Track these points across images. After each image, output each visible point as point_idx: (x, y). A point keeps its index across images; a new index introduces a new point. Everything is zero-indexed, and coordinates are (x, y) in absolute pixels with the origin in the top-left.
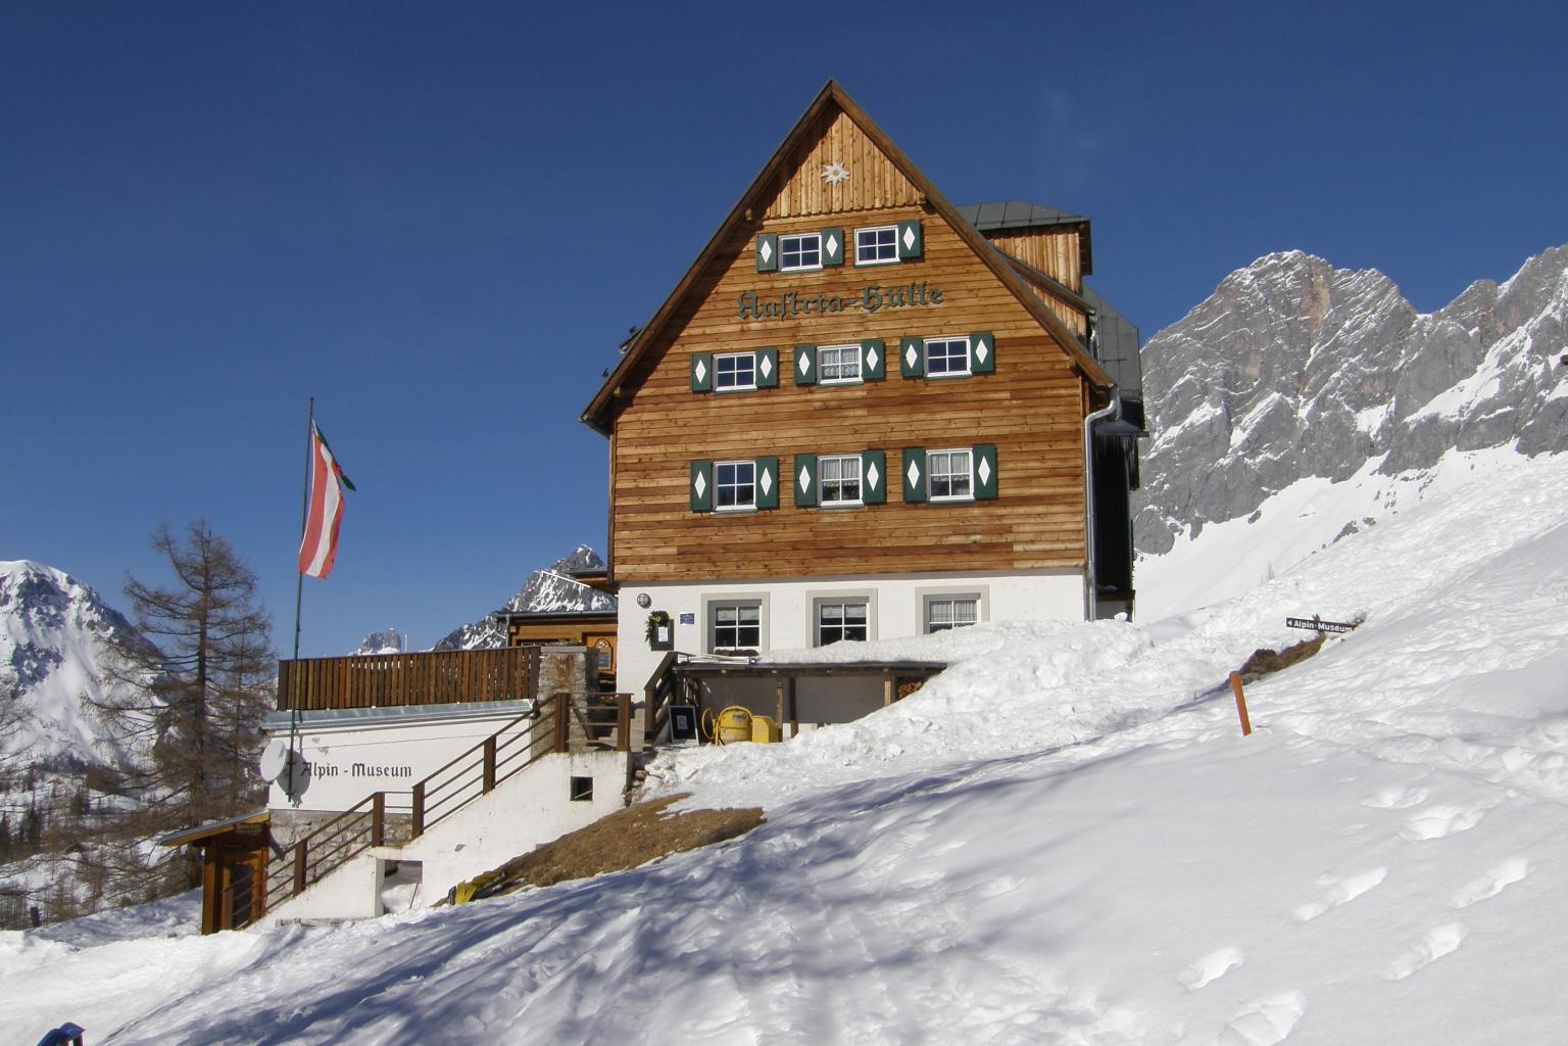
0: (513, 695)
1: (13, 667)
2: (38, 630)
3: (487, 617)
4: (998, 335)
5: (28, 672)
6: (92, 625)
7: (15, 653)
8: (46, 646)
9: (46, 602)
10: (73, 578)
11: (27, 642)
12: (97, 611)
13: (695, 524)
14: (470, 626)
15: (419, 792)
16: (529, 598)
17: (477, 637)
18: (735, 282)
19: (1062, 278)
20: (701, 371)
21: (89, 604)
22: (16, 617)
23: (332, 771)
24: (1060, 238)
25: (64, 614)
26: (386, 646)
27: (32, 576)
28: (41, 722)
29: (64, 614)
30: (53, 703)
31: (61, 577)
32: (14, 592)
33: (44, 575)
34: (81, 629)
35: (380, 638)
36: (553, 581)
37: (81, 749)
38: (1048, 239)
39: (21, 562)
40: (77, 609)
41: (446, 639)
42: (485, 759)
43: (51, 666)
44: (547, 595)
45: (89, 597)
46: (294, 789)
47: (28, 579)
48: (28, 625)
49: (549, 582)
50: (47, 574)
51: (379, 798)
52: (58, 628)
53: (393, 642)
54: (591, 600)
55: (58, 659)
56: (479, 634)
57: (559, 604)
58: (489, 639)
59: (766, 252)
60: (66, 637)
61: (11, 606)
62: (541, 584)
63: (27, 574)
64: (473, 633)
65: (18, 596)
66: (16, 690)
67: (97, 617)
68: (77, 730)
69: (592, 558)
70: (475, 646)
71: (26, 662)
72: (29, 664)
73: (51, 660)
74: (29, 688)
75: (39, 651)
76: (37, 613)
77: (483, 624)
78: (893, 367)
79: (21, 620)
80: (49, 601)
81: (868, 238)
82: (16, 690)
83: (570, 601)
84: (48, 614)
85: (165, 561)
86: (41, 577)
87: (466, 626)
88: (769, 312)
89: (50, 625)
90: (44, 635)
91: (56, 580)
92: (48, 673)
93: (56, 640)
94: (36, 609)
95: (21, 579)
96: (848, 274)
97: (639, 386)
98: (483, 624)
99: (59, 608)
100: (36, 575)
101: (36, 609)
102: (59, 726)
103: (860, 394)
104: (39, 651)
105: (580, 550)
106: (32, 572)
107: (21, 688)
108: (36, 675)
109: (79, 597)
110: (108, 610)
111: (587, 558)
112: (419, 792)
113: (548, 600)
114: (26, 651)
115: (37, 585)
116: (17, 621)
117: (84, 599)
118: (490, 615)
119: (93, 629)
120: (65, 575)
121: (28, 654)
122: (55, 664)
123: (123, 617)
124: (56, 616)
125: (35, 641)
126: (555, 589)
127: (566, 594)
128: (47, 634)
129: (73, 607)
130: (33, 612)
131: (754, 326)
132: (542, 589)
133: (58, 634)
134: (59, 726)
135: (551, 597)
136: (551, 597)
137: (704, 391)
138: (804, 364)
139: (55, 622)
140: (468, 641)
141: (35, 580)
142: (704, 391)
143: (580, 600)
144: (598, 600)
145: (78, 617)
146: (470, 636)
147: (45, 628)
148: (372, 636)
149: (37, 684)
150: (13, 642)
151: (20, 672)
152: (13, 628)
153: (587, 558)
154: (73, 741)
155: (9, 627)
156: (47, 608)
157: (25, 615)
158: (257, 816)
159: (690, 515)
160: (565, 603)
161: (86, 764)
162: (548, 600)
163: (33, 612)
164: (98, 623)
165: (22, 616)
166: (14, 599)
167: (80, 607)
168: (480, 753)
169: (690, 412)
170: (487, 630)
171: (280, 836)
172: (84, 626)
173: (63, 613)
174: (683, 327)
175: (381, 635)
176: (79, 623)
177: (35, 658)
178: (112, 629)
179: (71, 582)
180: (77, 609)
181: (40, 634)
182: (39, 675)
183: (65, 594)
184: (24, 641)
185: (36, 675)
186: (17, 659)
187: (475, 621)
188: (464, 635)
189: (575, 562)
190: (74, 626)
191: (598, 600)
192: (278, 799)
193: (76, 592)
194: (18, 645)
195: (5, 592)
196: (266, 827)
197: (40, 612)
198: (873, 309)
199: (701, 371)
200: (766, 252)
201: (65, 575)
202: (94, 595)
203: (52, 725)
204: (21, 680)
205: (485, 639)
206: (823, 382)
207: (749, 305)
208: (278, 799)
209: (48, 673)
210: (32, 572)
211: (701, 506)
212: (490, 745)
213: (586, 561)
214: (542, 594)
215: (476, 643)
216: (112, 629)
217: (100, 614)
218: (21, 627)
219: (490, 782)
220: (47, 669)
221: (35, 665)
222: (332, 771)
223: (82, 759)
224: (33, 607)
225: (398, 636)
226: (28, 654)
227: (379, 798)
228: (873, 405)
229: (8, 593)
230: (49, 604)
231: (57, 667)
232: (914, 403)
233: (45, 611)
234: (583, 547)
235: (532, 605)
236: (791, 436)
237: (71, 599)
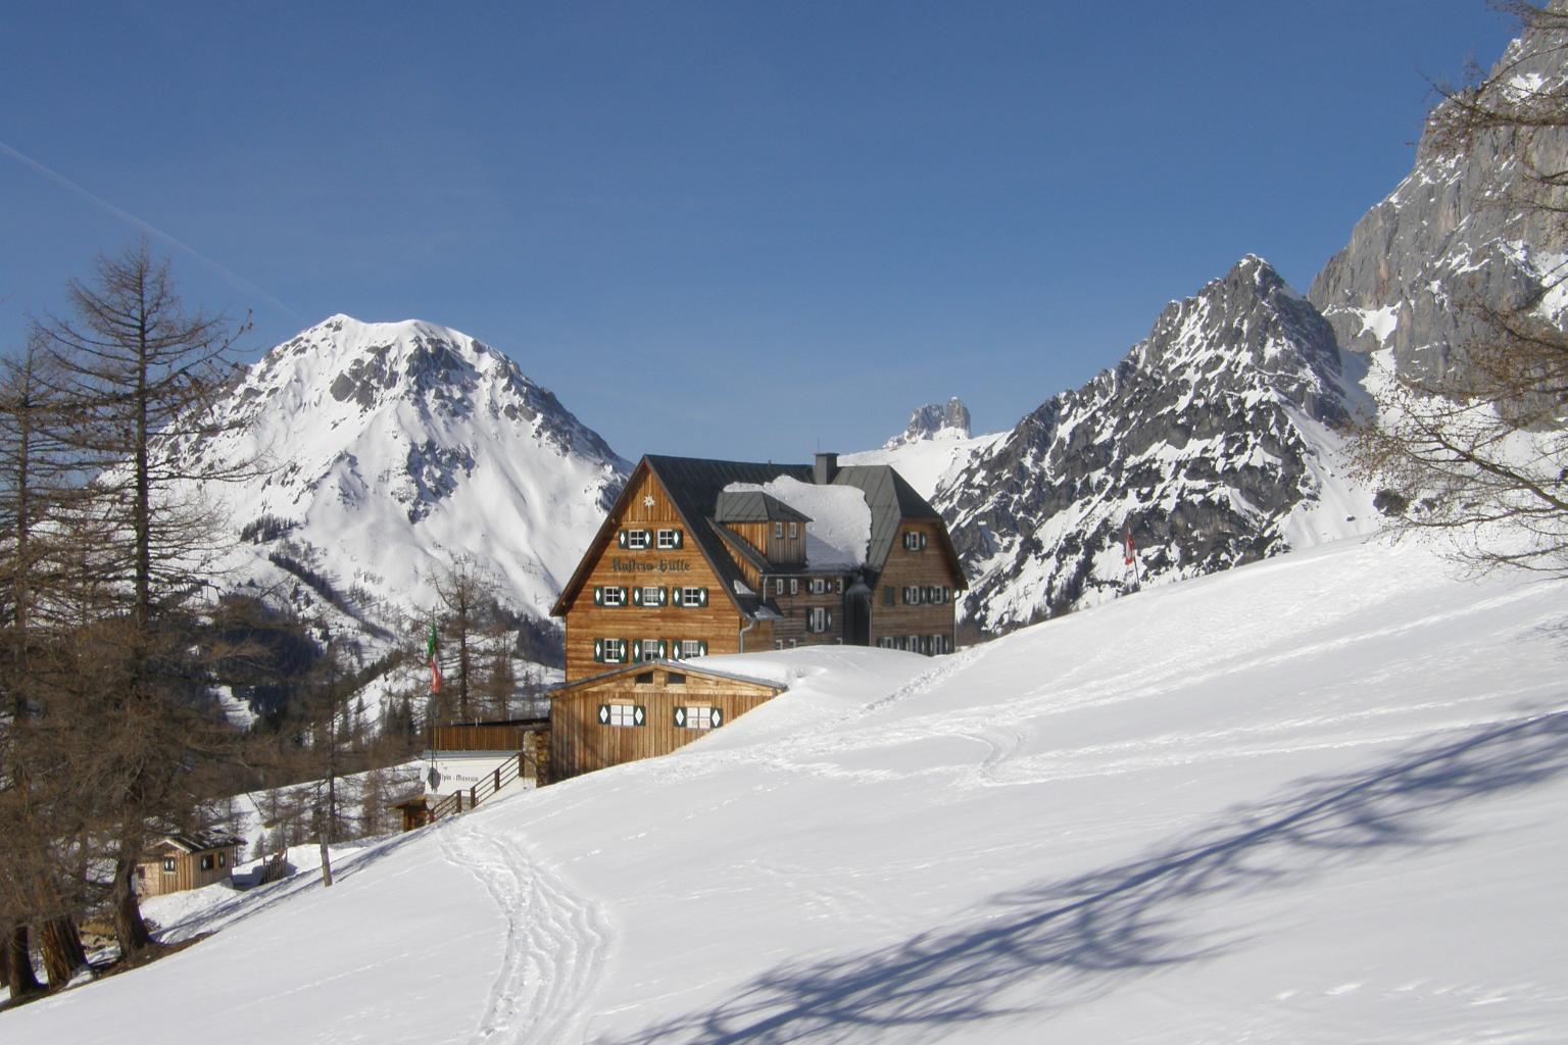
0: (514, 748)
1: (410, 477)
2: (439, 422)
3: (1096, 378)
4: (710, 588)
5: (430, 484)
6: (511, 411)
7: (410, 456)
8: (451, 445)
9: (447, 380)
10: (481, 343)
11: (425, 439)
12: (519, 391)
13: (597, 668)
14: (1070, 393)
15: (473, 790)
16: (1162, 344)
17: (1081, 410)
18: (611, 552)
19: (760, 548)
20: (598, 595)
21: (505, 381)
22: (407, 403)
23: (449, 778)
24: (760, 526)
25: (472, 396)
26: (947, 426)
27: (424, 343)
28: (452, 555)
29: (472, 396)
30: (467, 527)
31: (464, 342)
32: (402, 367)
33: (441, 341)
34: (497, 418)
35: (937, 413)
36: (1201, 317)
37: (508, 594)
38: (755, 526)
39: (409, 323)
40: (490, 389)
41: (1033, 415)
42: (520, 767)
43: (459, 473)
44: (1192, 339)
45: (504, 371)
46: (434, 785)
47: (420, 347)
48: (425, 414)
49: (1195, 317)
50: (445, 339)
51: (459, 792)
52: (466, 418)
53: (958, 419)
54: (1263, 345)
55: (469, 464)
56: (1084, 405)
57: (1212, 353)
58: (1099, 414)
59: (623, 538)
60: (477, 430)
61: (400, 388)
62: (1181, 322)
63: (418, 340)
64: (1075, 404)
65: (408, 373)
66: (415, 512)
67: (518, 400)
68: (501, 566)
69: (1265, 274)
70: (1078, 426)
71: (425, 470)
72: (430, 472)
73: (460, 466)
74: (433, 506)
75: (443, 453)
76: (436, 397)
77: (1090, 389)
78: (670, 600)
79: (415, 408)
80: (451, 378)
81: (663, 534)
82: (415, 512)
83: (1229, 348)
84: (451, 398)
85: (432, 589)
86: (437, 343)
87: (1064, 394)
88: (626, 568)
89: (454, 414)
90: (448, 430)
91: (458, 347)
92: (456, 484)
93: (462, 435)
94: (433, 392)
95: (410, 349)
96: (655, 553)
97: (575, 600)
98: (1090, 389)
99: (465, 389)
100: (431, 341)
101: (433, 392)
102: (476, 562)
103: (659, 611)
104: (443, 453)
105: (1245, 262)
106: (424, 338)
107: (421, 508)
108: (441, 488)
109: (492, 371)
110: (533, 389)
111: (1256, 275)
112: (473, 790)
113: (1193, 347)
114: (425, 453)
115: (433, 356)
116: (411, 411)
117: (499, 374)
118: (1101, 375)
119: (514, 418)
120: (470, 340)
121: (428, 457)
122: (465, 471)
123: (554, 397)
124: (461, 400)
125: (437, 439)
126: (1204, 328)
127: (1220, 336)
128: (451, 428)
129: (484, 386)
130: (430, 396)
131: (619, 574)
132: (1184, 329)
133: (467, 426)
134: (476, 562)
135: (1198, 342)
136: (1198, 342)
137: (601, 604)
138: (637, 596)
139: (460, 410)
140: (1067, 417)
141: (430, 349)
142: (601, 604)
143: (1245, 346)
144: (1276, 345)
145: (492, 402)
146: (1071, 410)
147: (448, 419)
148: (925, 410)
149: (443, 500)
150: (407, 441)
151: (419, 484)
152: (405, 420)
153: (1256, 275)
154: (496, 583)
155: (399, 420)
156: (448, 389)
157: (419, 401)
158: (421, 798)
159: (595, 663)
160: (1221, 351)
161: (516, 616)
162: (1193, 347)
163: (430, 396)
164: (521, 409)
165: (416, 402)
166: (403, 377)
167: (493, 386)
168: (493, 776)
169: (595, 612)
170: (1097, 399)
171: (430, 806)
172: (501, 414)
173: (470, 395)
174: (591, 572)
175: (939, 408)
176: (494, 410)
177: (438, 463)
178: (540, 416)
179: (479, 349)
180: (490, 389)
181: (442, 428)
182: (445, 487)
183: (472, 367)
184: (422, 439)
185: (441, 488)
186: (414, 466)
187: (1077, 386)
188: (1060, 408)
189: (1236, 283)
190: (488, 414)
191: (1276, 345)
192: (428, 789)
193: (487, 363)
194: (413, 444)
195: (391, 368)
196: (424, 802)
197: (439, 395)
198: (663, 570)
199: (598, 595)
200: (623, 538)
201: (470, 340)
202: (512, 366)
203: (466, 560)
204: (421, 495)
205: (1094, 415)
206: (646, 604)
207: (617, 564)
208: (428, 789)
209: (456, 484)
210: (424, 338)
211: (601, 659)
212: (497, 773)
213: (1254, 281)
214: (1183, 339)
215: (1080, 420)
216: (540, 416)
217: (521, 394)
218: (416, 418)
219: (497, 787)
220: (454, 477)
221: (438, 473)
222: (449, 778)
223: (510, 608)
224: (431, 388)
225: (965, 410)
226: (428, 457)
227: (459, 792)
228: (663, 617)
229: (395, 369)
230: (451, 384)
231: (468, 475)
232: (677, 618)
233: (446, 394)
234: (1249, 258)
235: (1167, 356)
236: (632, 629)
237: (480, 375)
